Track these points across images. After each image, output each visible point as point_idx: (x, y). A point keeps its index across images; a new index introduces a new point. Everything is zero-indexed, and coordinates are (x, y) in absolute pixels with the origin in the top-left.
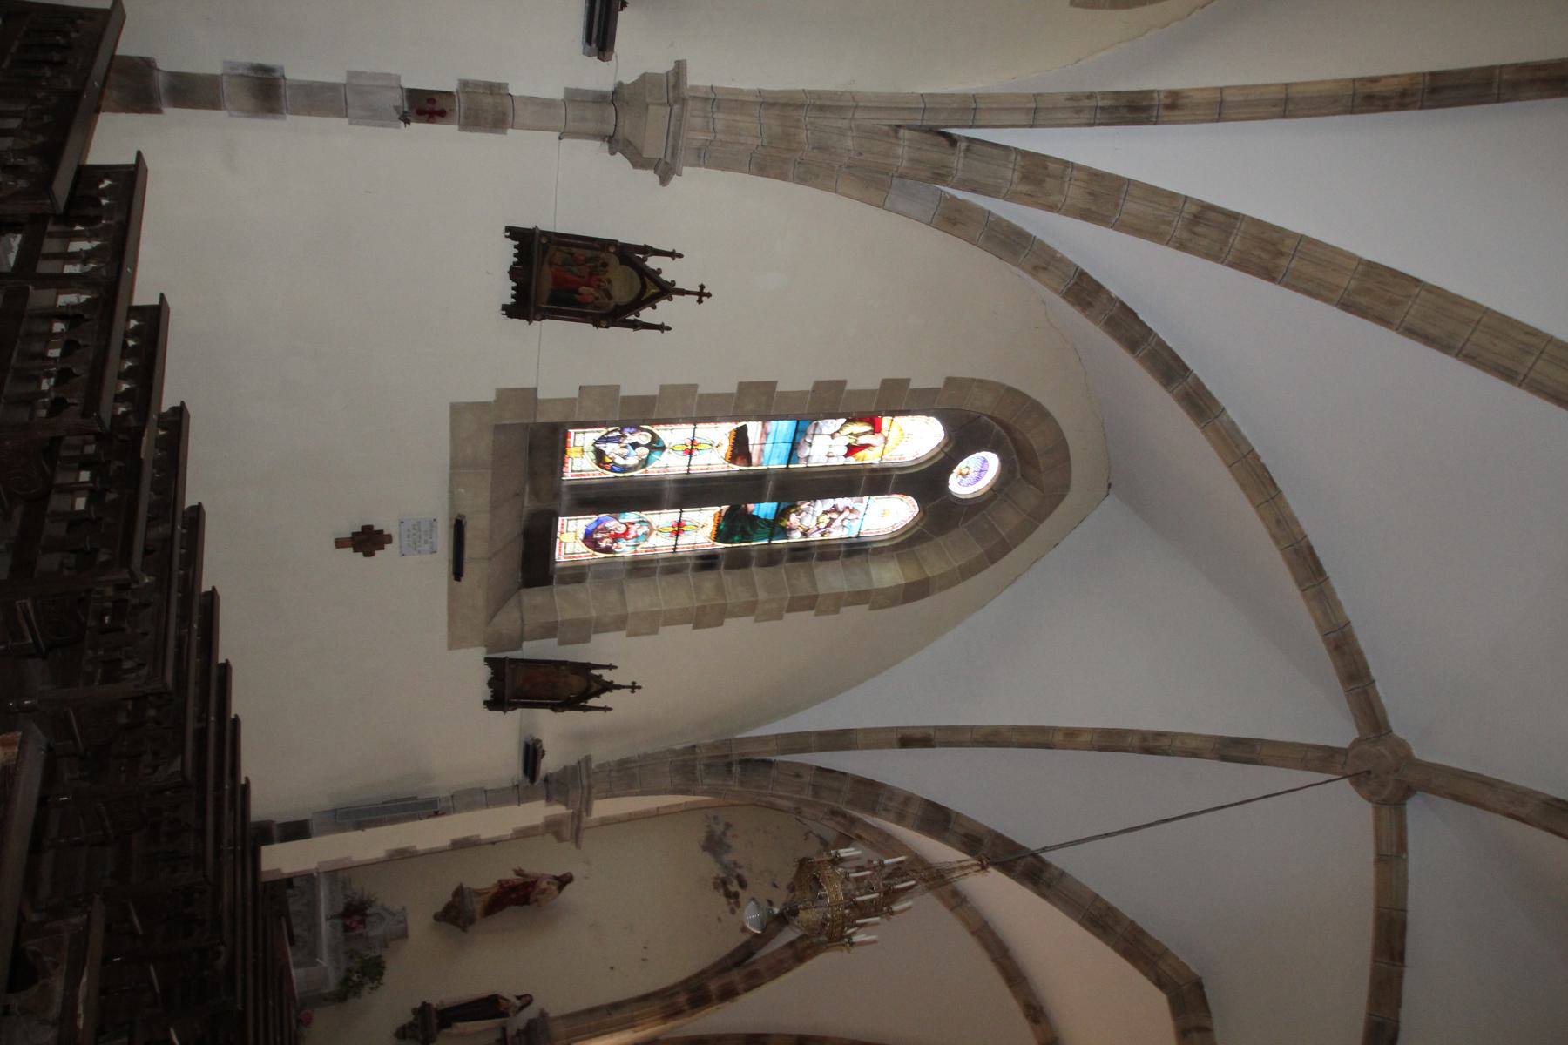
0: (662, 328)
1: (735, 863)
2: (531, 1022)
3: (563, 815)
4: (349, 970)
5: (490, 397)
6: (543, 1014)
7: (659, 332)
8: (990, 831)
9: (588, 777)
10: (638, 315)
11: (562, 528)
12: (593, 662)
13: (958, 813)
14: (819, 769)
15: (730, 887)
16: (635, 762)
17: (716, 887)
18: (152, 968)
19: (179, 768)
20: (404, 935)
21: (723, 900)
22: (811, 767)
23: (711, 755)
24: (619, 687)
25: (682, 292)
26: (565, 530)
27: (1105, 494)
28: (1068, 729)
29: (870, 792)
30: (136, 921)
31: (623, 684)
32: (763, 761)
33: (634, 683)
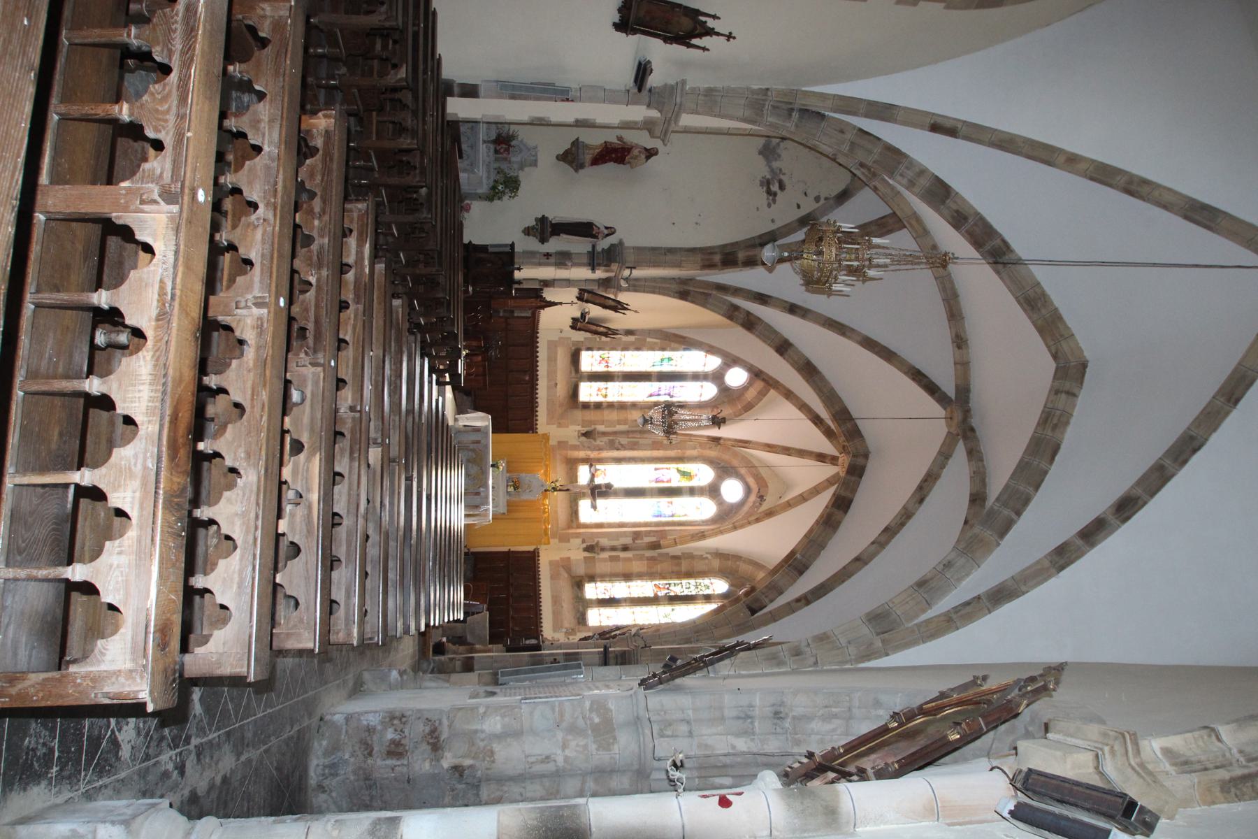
1: (781, 170)
2: (612, 246)
3: (658, 118)
4: (496, 181)
6: (621, 243)
8: (977, 214)
9: (682, 97)
12: (702, 10)
13: (957, 193)
14: (861, 130)
15: (772, 187)
16: (719, 91)
17: (762, 184)
19: (404, 76)
20: (534, 164)
21: (765, 195)
22: (855, 127)
23: (778, 99)
24: (718, 34)
28: (1073, 154)
29: (894, 156)
30: (375, 163)
31: (722, 32)
32: (819, 113)
33: (730, 33)
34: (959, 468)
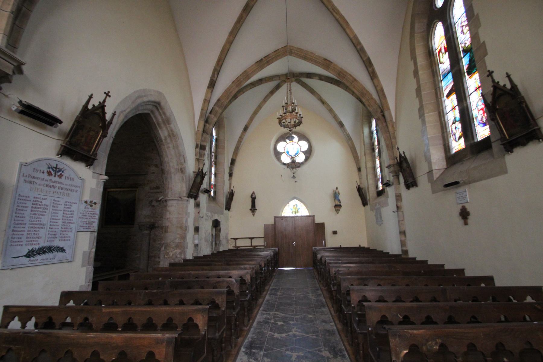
0: (508, 76)
5: (430, 184)
7: (92, 99)
10: (107, 120)
25: (104, 101)
31: (104, 99)
34: (313, 83)
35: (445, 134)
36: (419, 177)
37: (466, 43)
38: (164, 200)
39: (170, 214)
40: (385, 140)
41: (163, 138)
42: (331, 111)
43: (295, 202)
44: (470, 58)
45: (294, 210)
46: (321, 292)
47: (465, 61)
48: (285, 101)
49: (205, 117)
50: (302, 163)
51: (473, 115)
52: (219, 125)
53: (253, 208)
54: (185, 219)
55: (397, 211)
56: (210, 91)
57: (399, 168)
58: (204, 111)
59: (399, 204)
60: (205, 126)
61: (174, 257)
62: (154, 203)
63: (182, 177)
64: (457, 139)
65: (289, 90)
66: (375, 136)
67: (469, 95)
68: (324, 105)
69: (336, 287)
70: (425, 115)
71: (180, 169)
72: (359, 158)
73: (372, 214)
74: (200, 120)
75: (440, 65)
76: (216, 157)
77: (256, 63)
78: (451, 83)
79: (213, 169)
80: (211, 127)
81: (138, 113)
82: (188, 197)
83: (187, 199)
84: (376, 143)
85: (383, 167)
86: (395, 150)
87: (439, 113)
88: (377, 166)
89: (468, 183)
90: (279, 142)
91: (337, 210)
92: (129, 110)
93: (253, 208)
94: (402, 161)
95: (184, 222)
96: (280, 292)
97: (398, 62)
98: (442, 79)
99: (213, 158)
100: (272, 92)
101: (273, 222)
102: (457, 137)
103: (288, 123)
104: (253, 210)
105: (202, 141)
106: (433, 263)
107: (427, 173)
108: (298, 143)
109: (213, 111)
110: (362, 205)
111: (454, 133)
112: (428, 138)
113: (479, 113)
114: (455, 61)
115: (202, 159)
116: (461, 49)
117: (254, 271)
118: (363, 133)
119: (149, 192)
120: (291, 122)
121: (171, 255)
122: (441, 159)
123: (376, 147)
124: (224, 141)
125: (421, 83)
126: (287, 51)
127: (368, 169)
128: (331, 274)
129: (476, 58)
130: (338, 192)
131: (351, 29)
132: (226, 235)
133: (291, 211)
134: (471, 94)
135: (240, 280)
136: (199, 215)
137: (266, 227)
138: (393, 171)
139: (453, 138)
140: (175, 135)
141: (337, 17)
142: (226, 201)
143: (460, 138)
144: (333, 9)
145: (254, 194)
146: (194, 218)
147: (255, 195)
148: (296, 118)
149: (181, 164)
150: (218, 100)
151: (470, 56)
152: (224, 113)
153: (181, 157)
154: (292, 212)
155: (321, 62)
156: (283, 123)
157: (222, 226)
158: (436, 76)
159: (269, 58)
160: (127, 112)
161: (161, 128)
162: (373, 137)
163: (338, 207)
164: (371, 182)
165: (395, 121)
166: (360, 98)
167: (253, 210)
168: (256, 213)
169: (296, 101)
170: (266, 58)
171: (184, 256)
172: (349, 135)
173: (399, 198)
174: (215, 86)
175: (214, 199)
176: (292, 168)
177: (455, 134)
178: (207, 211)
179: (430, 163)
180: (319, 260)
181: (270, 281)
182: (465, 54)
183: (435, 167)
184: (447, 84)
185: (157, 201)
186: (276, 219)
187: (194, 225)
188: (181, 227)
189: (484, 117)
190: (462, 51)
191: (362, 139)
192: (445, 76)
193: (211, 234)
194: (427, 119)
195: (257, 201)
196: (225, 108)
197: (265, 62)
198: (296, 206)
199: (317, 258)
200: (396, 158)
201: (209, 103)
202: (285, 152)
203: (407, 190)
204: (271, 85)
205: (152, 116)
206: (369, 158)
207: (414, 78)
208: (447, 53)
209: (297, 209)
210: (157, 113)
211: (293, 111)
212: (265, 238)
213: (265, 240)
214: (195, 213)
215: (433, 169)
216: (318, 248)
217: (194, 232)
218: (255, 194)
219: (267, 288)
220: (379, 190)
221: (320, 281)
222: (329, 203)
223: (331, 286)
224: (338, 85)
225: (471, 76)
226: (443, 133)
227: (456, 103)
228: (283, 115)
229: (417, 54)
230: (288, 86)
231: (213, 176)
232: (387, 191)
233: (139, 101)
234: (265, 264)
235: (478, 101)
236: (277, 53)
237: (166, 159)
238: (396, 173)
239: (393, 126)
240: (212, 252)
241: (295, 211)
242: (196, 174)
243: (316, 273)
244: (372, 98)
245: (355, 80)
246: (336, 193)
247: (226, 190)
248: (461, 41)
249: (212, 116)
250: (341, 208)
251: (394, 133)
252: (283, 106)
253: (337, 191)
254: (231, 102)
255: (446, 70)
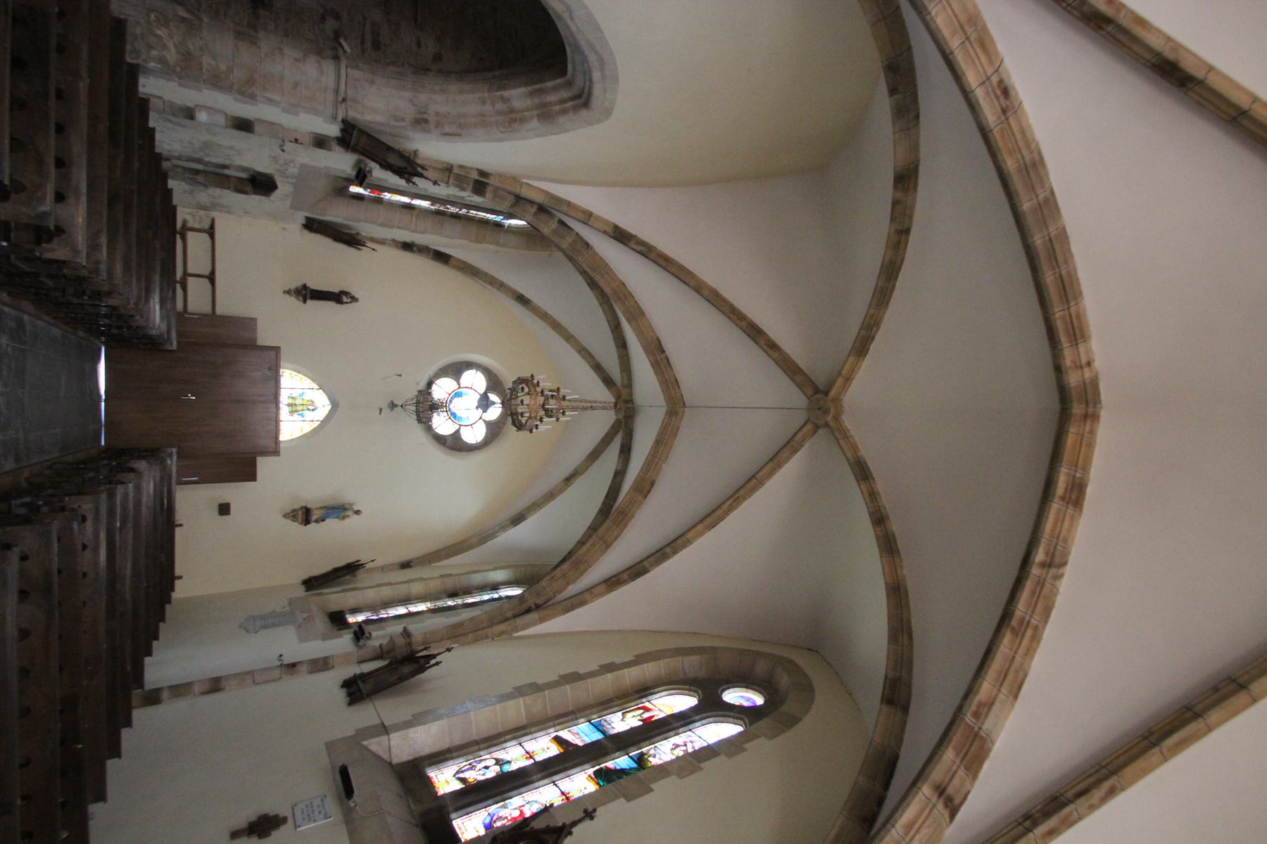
5: (353, 733)
11: (460, 830)
18: (103, 443)
26: (463, 830)
27: (815, 653)
34: (611, 457)
35: (477, 747)
36: (375, 706)
37: (654, 756)
38: (341, 51)
39: (297, 60)
40: (472, 619)
41: (506, 93)
42: (551, 496)
43: (323, 405)
44: (625, 769)
45: (298, 402)
46: (7, 469)
47: (622, 762)
48: (571, 394)
49: (553, 208)
50: (429, 429)
51: (511, 798)
52: (532, 237)
53: (307, 294)
54: (276, 97)
55: (281, 665)
56: (609, 230)
57: (399, 657)
58: (565, 208)
59: (304, 668)
60: (532, 202)
61: (152, 40)
62: (331, 24)
63: (403, 120)
64: (461, 775)
65: (593, 404)
66: (486, 597)
67: (554, 782)
68: (563, 481)
69: (23, 511)
70: (521, 699)
71: (425, 116)
72: (434, 563)
73: (279, 604)
74: (547, 193)
75: (620, 714)
76: (455, 216)
77: (658, 340)
78: (583, 741)
79: (425, 204)
80: (530, 218)
81: (568, 49)
82: (344, 121)
83: (340, 118)
84: (470, 600)
85: (409, 620)
86: (447, 644)
87: (524, 727)
88: (413, 605)
89: (349, 819)
90: (486, 377)
91: (295, 513)
92: (574, 29)
93: (307, 294)
94: (417, 662)
95: (268, 95)
96: (7, 345)
97: (634, 631)
98: (592, 721)
99: (453, 210)
100: (598, 368)
101: (264, 344)
102: (466, 775)
103: (520, 399)
104: (304, 292)
105: (497, 189)
106: (109, 773)
107: (383, 723)
108: (481, 420)
109: (565, 228)
110: (306, 576)
111: (475, 766)
112: (469, 711)
113: (515, 809)
114: (623, 742)
115: (451, 181)
116: (644, 750)
117: (84, 273)
118: (496, 569)
119: (365, 19)
120: (523, 406)
121: (158, 32)
122: (415, 749)
123: (459, 601)
124: (497, 244)
125: (589, 680)
126: (674, 406)
127: (406, 586)
128: (73, 498)
129: (624, 781)
130: (348, 516)
131: (701, 534)
132: (227, 207)
133: (298, 395)
134: (556, 785)
135: (48, 227)
136: (291, 141)
137: (249, 324)
138: (394, 643)
139: (464, 767)
140: (513, 125)
141: (725, 506)
142: (331, 223)
143: (463, 780)
144: (738, 498)
145: (349, 300)
146: (281, 125)
147: (346, 303)
148: (530, 418)
149: (438, 125)
150: (587, 245)
151: (631, 769)
152: (560, 254)
153: (457, 129)
154: (294, 396)
155: (649, 475)
156: (523, 388)
157: (254, 200)
158: (600, 708)
159: (665, 367)
160: (569, 22)
161: (531, 94)
162: (485, 593)
163: (305, 516)
164: (371, 595)
165: (515, 637)
166: (571, 557)
167: (304, 292)
168: (293, 299)
169: (569, 419)
170: (665, 361)
171: (151, 70)
172: (493, 539)
173: (321, 665)
174: (616, 242)
175: (340, 190)
176: (418, 403)
177: (472, 768)
178: (302, 166)
179: (408, 725)
180: (128, 465)
181: (55, 318)
182: (636, 759)
183: (395, 738)
184: (581, 734)
185: (337, 35)
186: (272, 353)
187: (258, 120)
188: (251, 81)
189: (506, 820)
190: (642, 752)
191: (481, 569)
192: (598, 727)
193: (227, 162)
194: (511, 703)
195: (329, 306)
196: (570, 258)
197: (659, 359)
198: (311, 406)
199: (138, 459)
200: (425, 649)
201: (583, 223)
202: (460, 388)
203: (342, 681)
204: (613, 366)
205: (559, 81)
206: (434, 585)
207: (601, 666)
208: (641, 723)
209: (303, 410)
210: (564, 94)
211: (546, 411)
212: (213, 318)
213: (204, 315)
214: (296, 130)
215: (392, 736)
216: (173, 463)
217: (234, 115)
218: (351, 302)
219: (27, 306)
220: (347, 616)
221: (50, 467)
222: (313, 494)
223: (28, 499)
224: (601, 510)
225: (592, 778)
226: (477, 743)
227: (540, 757)
228: (539, 389)
229: (645, 665)
230: (601, 403)
231: (406, 200)
232: (341, 636)
233: (592, 58)
234: (114, 308)
235: (540, 803)
236: (672, 383)
237: (453, 87)
238: (388, 652)
239: (503, 633)
240: (163, 156)
241: (296, 405)
242: (412, 157)
243: (80, 456)
244: (568, 584)
245: (608, 546)
246: (345, 509)
247: (366, 229)
248: (659, 747)
249: (554, 225)
250: (301, 523)
251: (487, 637)
252: (558, 389)
253: (350, 513)
254: (583, 273)
255: (609, 727)
